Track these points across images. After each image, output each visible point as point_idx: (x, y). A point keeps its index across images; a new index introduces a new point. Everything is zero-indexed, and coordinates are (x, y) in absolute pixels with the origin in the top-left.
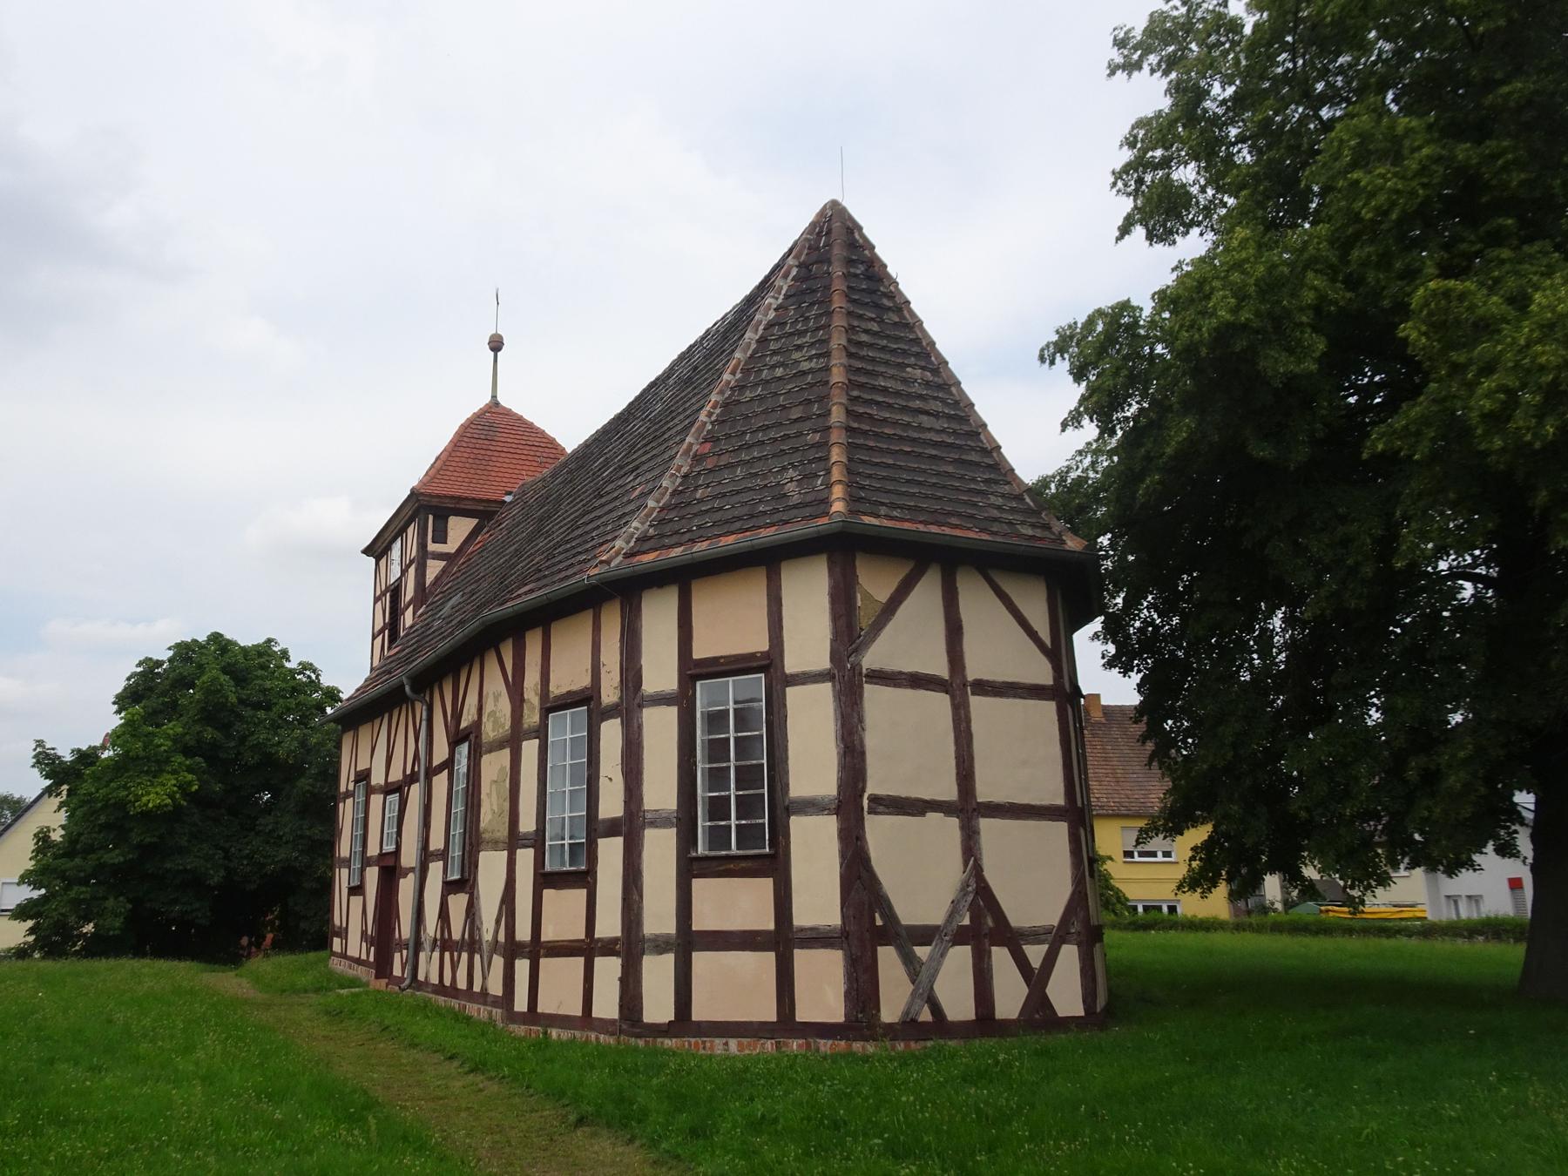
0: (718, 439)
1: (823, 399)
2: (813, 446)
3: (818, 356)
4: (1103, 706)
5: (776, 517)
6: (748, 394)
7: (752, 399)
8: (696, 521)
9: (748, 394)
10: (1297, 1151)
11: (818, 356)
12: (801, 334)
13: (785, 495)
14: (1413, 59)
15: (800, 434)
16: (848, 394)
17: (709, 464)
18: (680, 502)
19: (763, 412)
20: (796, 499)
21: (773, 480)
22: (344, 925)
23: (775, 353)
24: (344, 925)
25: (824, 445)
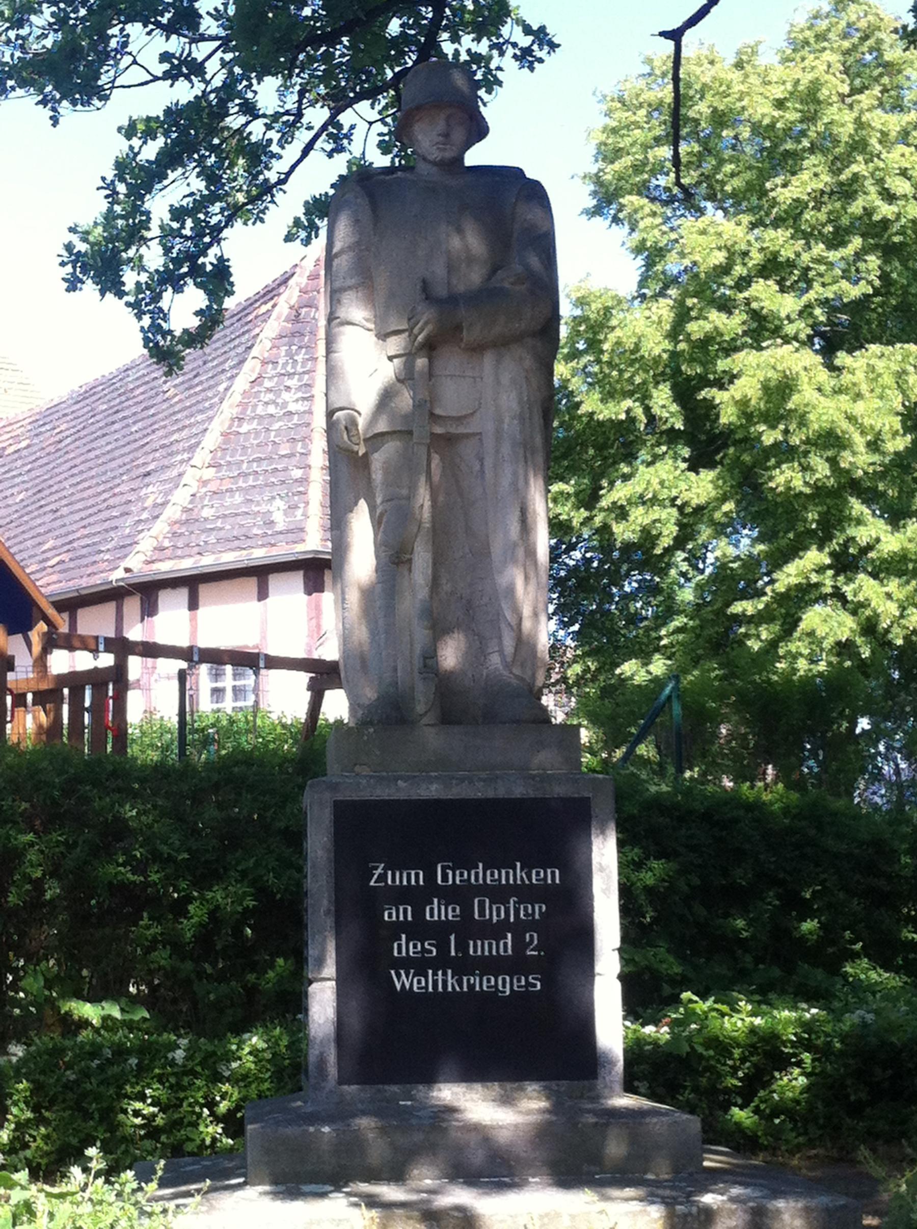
0: (221, 465)
1: (306, 439)
2: (296, 481)
3: (304, 399)
4: (340, 687)
5: (266, 540)
6: (245, 428)
7: (249, 432)
8: (203, 537)
9: (245, 428)
10: (718, 589)
11: (304, 399)
12: (290, 375)
13: (272, 522)
14: (17, 993)
15: (286, 469)
16: (197, 663)
17: (213, 487)
18: (190, 519)
19: (258, 445)
20: (280, 527)
21: (264, 508)
22: (443, 908)
23: (269, 390)
24: (443, 908)
25: (304, 481)
